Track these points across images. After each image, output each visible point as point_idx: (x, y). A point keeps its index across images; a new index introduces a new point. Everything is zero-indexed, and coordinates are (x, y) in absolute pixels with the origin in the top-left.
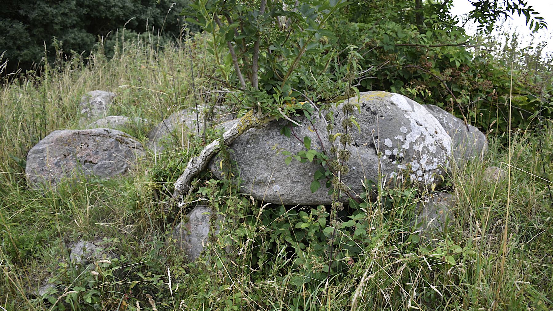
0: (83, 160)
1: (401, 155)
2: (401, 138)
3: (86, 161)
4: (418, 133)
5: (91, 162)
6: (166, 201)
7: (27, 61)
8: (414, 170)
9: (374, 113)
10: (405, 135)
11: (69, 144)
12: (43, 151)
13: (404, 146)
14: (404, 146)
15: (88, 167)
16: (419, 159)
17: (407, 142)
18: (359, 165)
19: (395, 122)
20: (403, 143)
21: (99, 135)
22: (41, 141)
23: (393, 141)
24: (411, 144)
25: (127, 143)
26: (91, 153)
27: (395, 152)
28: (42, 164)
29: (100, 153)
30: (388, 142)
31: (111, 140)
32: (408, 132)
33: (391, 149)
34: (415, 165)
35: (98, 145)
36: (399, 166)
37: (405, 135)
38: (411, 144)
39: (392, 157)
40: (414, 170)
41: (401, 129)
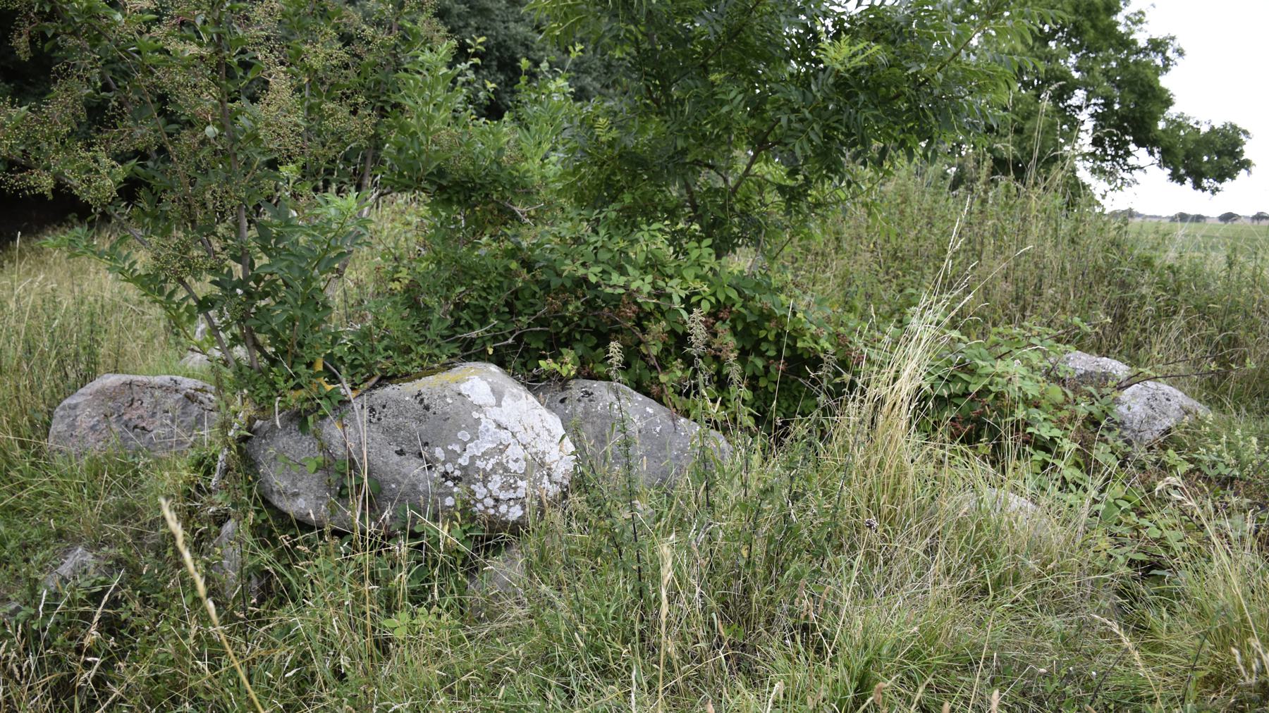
0: (132, 425)
1: (457, 473)
2: (457, 448)
3: (136, 427)
4: (493, 442)
5: (143, 428)
6: (41, 525)
7: (405, 188)
8: (478, 496)
9: (427, 408)
10: (466, 443)
11: (113, 399)
12: (75, 407)
13: (460, 461)
14: (460, 461)
15: (137, 436)
16: (485, 481)
17: (467, 455)
18: (399, 483)
19: (462, 418)
20: (460, 456)
21: (161, 387)
22: (81, 391)
23: (446, 451)
24: (473, 458)
25: (201, 402)
26: (145, 415)
27: (449, 468)
28: (72, 426)
29: (158, 416)
30: (439, 453)
31: (180, 396)
32: (471, 440)
33: (444, 463)
34: (480, 491)
35: (156, 404)
36: (455, 489)
37: (466, 443)
38: (473, 458)
39: (445, 475)
40: (478, 496)
41: (459, 434)
